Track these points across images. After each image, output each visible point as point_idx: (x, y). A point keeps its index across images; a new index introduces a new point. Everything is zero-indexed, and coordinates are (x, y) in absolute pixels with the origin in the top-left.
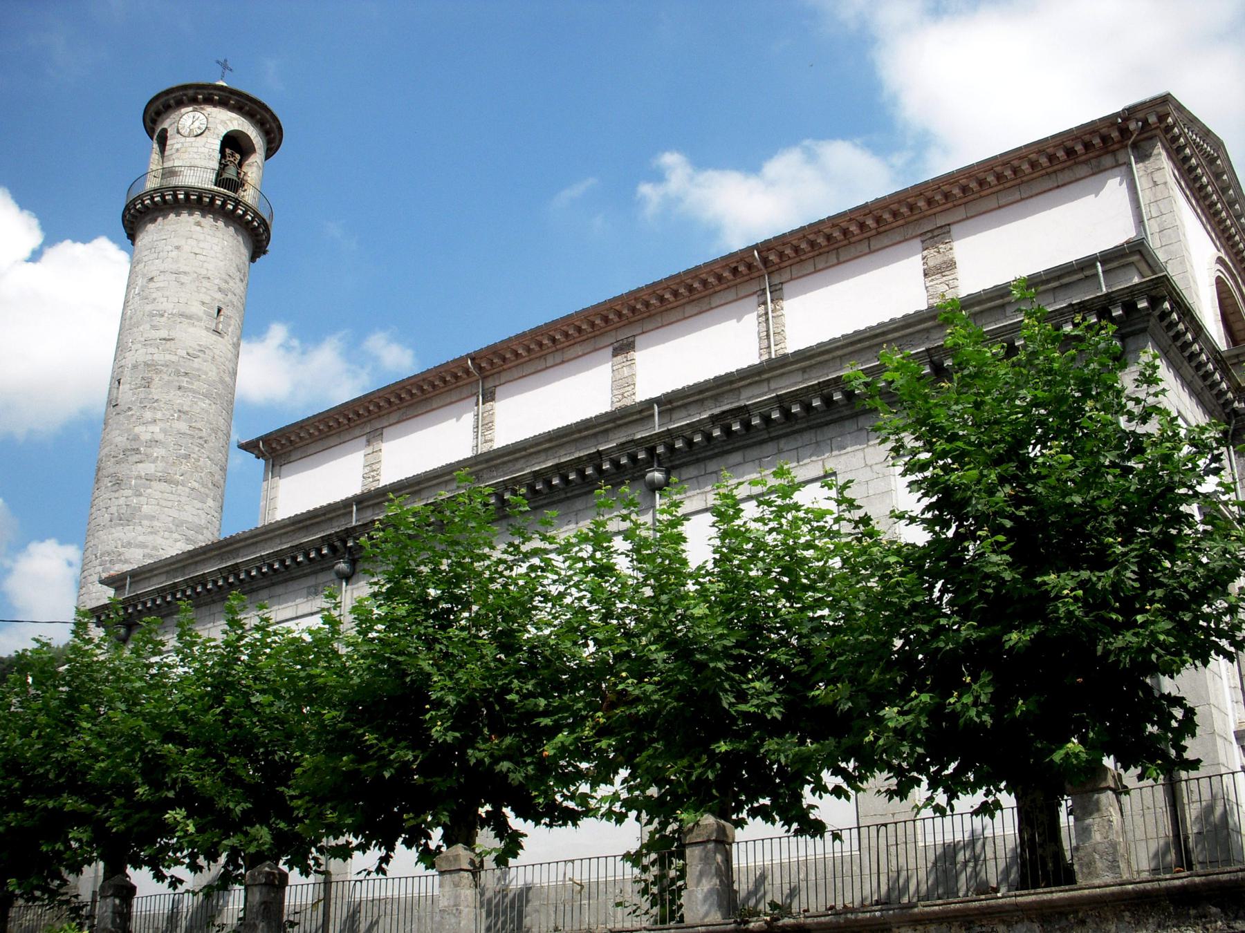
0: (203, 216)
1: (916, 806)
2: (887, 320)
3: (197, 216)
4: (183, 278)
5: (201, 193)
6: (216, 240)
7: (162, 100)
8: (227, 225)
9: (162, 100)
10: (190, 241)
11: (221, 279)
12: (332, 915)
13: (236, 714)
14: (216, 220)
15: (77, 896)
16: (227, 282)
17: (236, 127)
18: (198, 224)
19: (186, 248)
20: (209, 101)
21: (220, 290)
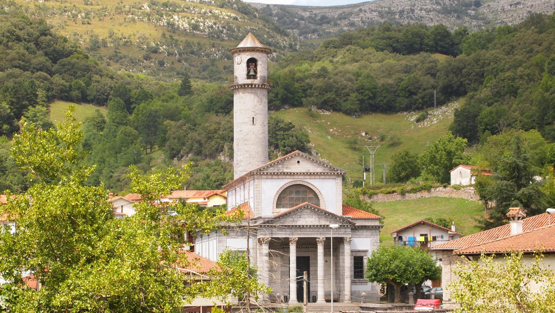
21: (252, 112)
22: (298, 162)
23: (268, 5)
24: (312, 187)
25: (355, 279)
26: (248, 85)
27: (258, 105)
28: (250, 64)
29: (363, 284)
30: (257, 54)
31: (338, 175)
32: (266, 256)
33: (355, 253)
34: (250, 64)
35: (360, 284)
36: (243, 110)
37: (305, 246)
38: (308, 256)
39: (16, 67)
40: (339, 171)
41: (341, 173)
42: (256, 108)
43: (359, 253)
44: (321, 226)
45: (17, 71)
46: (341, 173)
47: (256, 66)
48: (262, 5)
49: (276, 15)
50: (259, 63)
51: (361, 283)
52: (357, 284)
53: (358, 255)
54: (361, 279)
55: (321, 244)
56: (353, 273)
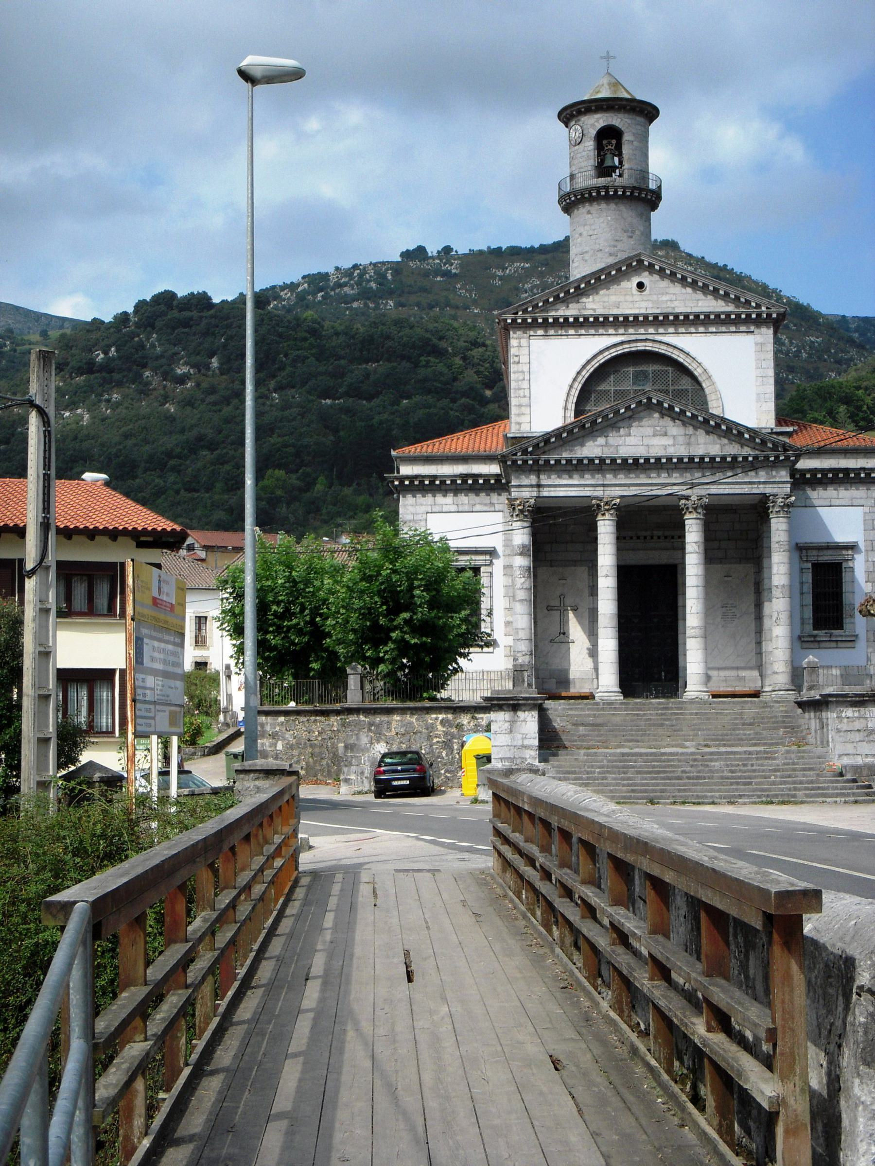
0: (591, 205)
1: (609, 1157)
2: (536, 246)
3: (587, 207)
4: (587, 257)
5: (589, 190)
6: (602, 220)
7: (568, 111)
8: (608, 204)
9: (568, 111)
10: (586, 227)
11: (610, 246)
12: (558, 489)
13: (279, 428)
14: (599, 204)
15: (489, 635)
16: (615, 246)
17: (602, 124)
18: (589, 212)
19: (585, 233)
20: (580, 113)
21: (611, 255)
22: (640, 286)
23: (844, 316)
24: (681, 358)
25: (816, 632)
26: (598, 189)
27: (625, 239)
28: (604, 142)
29: (840, 645)
30: (621, 115)
31: (760, 322)
32: (521, 554)
33: (814, 553)
34: (604, 142)
35: (834, 645)
36: (586, 252)
37: (660, 533)
38: (671, 561)
39: (429, 392)
40: (764, 309)
41: (769, 315)
42: (620, 246)
43: (830, 552)
44: (691, 459)
45: (430, 399)
46: (769, 315)
47: (619, 147)
48: (835, 316)
49: (856, 331)
50: (627, 137)
51: (837, 643)
52: (823, 645)
53: (827, 557)
54: (835, 632)
55: (694, 515)
56: (809, 613)
